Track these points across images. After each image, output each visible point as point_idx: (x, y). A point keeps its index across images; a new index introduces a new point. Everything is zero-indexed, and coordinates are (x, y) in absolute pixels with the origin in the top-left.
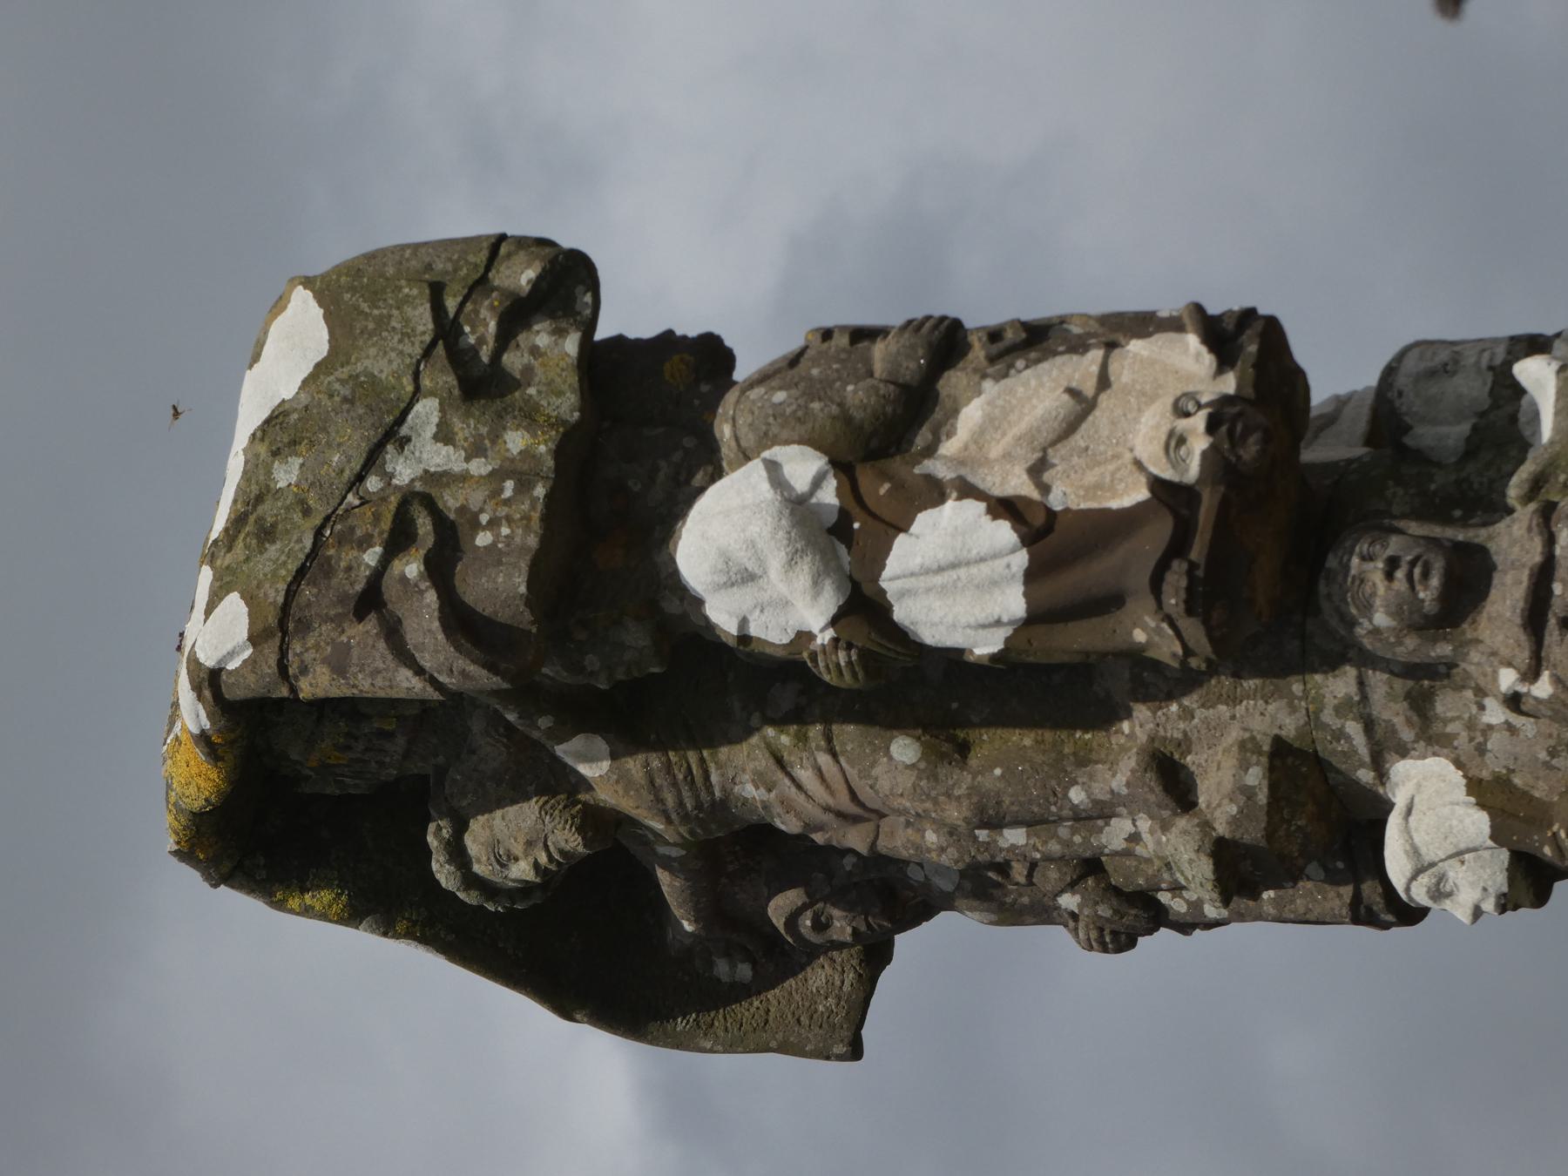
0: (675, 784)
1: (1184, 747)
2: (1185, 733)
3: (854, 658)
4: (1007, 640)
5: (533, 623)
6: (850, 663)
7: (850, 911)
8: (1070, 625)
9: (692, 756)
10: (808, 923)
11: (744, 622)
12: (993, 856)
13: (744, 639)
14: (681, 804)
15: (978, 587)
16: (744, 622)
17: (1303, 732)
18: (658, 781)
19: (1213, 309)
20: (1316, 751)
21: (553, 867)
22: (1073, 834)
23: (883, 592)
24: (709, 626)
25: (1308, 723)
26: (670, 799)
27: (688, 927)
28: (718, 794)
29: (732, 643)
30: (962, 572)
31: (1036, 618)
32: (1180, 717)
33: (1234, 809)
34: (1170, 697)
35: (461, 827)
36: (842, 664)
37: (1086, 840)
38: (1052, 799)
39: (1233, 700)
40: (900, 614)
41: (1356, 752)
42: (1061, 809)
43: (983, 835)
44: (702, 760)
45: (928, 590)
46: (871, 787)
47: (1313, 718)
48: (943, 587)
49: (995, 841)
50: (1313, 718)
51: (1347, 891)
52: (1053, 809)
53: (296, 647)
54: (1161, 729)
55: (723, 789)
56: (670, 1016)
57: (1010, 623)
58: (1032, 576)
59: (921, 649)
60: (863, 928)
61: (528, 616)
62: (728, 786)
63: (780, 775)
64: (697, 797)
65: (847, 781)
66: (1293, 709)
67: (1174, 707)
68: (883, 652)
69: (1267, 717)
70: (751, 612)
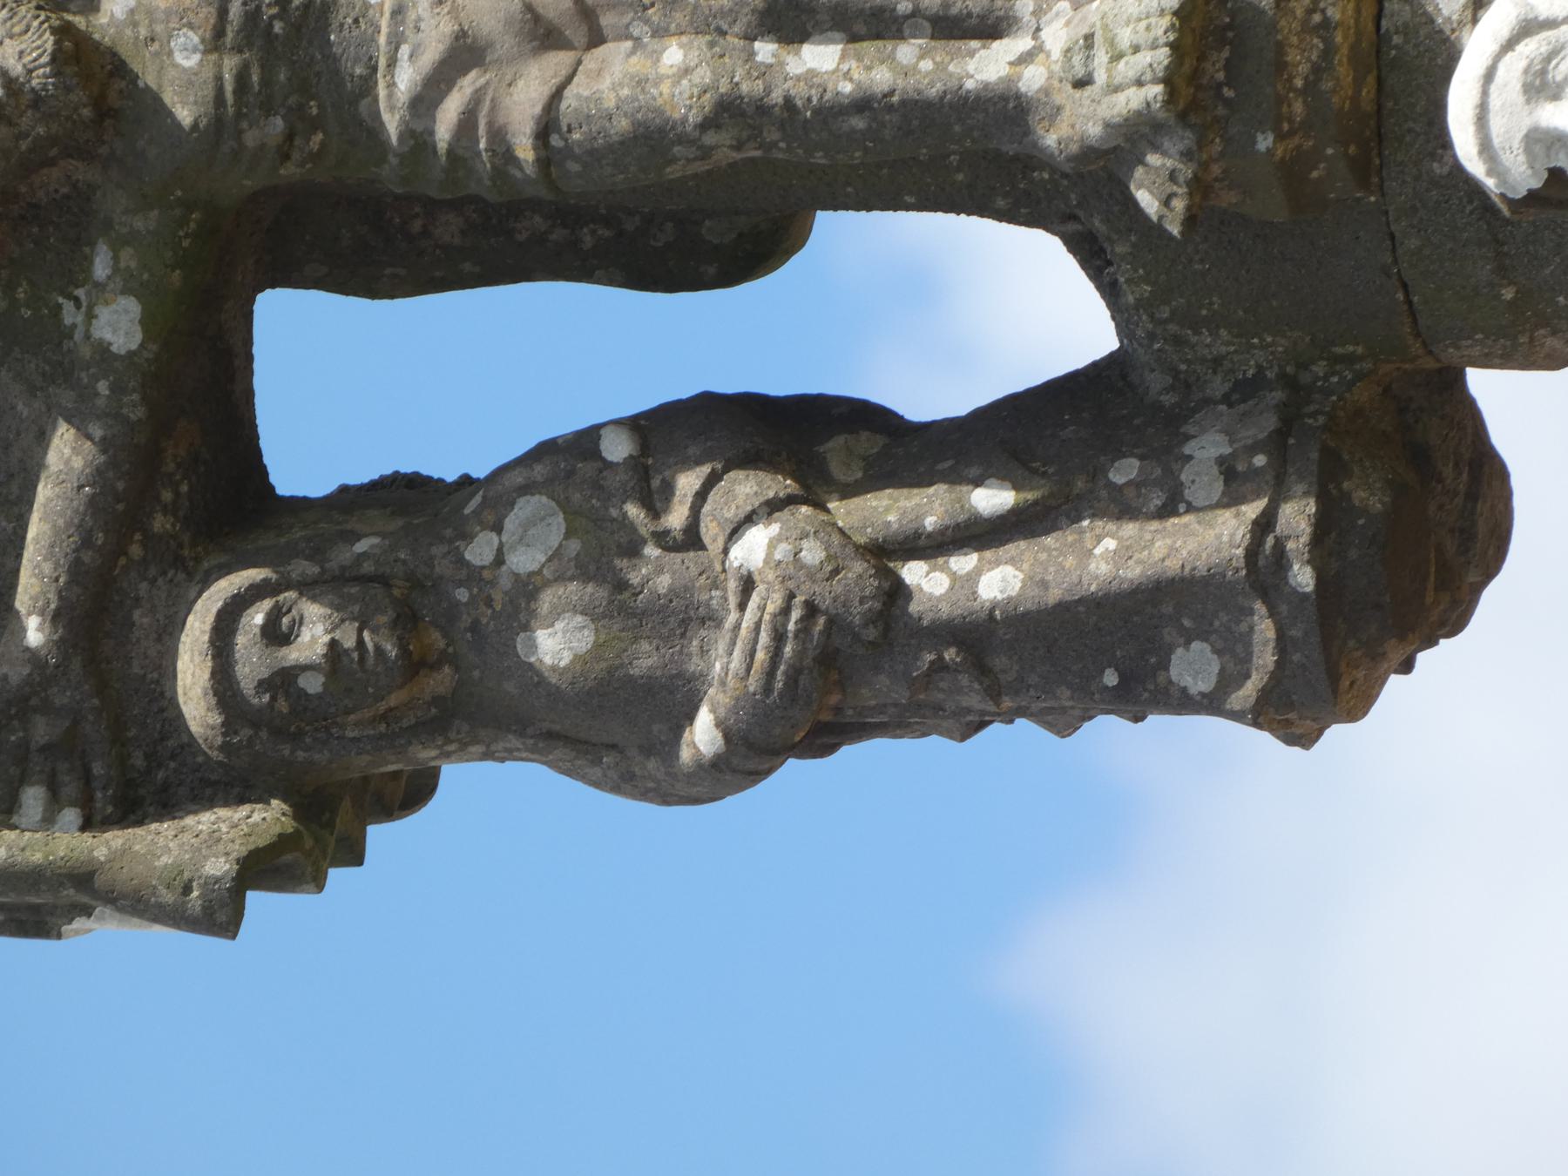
27: (35, 633)
43: (765, 50)
51: (1252, 510)
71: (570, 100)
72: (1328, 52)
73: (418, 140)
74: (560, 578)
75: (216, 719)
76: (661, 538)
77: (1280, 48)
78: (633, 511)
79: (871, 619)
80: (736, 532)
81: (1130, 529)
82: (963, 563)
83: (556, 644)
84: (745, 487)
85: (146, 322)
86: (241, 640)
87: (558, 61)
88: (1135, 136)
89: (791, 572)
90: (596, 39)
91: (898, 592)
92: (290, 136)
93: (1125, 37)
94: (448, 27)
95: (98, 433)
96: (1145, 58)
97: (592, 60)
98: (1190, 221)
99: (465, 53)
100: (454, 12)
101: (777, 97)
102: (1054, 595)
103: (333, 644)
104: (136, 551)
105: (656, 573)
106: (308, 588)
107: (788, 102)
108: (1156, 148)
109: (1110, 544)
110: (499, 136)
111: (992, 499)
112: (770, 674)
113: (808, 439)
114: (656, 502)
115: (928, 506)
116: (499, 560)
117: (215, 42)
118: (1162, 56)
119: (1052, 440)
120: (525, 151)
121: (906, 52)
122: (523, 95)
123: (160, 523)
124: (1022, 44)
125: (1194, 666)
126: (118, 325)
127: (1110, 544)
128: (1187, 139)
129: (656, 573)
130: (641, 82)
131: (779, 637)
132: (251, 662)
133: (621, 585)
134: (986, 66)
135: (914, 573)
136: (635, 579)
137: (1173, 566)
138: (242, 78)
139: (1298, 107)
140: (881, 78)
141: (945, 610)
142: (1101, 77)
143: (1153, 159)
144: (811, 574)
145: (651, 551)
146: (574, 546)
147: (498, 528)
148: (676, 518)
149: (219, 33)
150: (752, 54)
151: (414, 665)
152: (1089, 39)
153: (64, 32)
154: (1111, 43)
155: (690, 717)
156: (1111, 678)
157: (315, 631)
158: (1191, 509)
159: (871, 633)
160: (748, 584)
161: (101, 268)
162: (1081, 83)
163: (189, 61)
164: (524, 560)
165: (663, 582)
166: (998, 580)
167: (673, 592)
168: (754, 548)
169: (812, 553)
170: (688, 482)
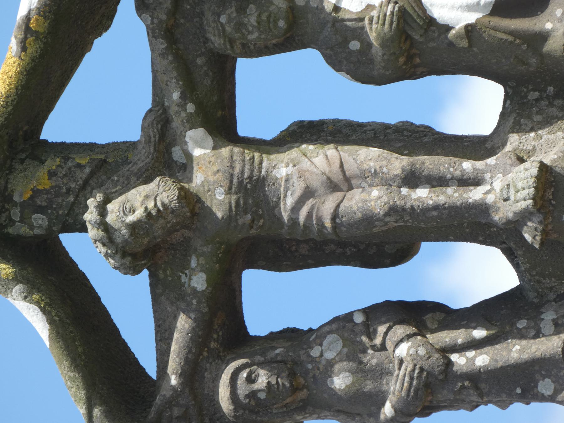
0: (243, 161)
2: (534, 147)
4: (478, 20)
6: (392, 13)
7: (270, 371)
8: (513, 20)
9: (257, 155)
10: (245, 375)
12: (405, 204)
14: (242, 172)
18: (235, 157)
21: (154, 213)
22: (455, 192)
26: (238, 167)
28: (263, 173)
34: (532, 130)
35: (108, 200)
36: (388, 13)
37: (461, 195)
38: (452, 164)
43: (404, 191)
44: (261, 156)
46: (354, 159)
49: (410, 195)
52: (452, 170)
54: (522, 145)
56: (237, 143)
57: (486, 5)
59: (431, 21)
60: (274, 382)
62: (270, 170)
63: (304, 158)
64: (252, 171)
65: (341, 158)
67: (532, 134)
68: (411, 12)
73: (294, 221)
74: (341, 360)
75: (232, 407)
76: (373, 347)
78: (364, 339)
79: (441, 372)
80: (397, 345)
81: (524, 342)
82: (471, 354)
83: (340, 382)
84: (400, 331)
85: (208, 281)
86: (239, 382)
87: (338, 196)
88: (524, 216)
89: (415, 357)
90: (350, 188)
91: (449, 364)
92: (253, 221)
93: (520, 185)
94: (303, 185)
95: (193, 316)
96: (526, 191)
97: (349, 195)
98: (542, 243)
99: (308, 193)
100: (305, 180)
101: (408, 205)
102: (500, 364)
103: (269, 383)
104: (205, 354)
105: (372, 358)
106: (261, 365)
108: (531, 220)
109: (518, 347)
110: (320, 220)
111: (479, 333)
112: (409, 390)
113: (420, 315)
114: (371, 335)
115: (459, 336)
116: (321, 355)
117: (229, 191)
118: (532, 191)
119: (499, 315)
120: (328, 224)
121: (450, 190)
122: (327, 206)
123: (213, 345)
125: (546, 386)
126: (199, 282)
127: (518, 347)
128: (541, 217)
129: (372, 358)
130: (365, 201)
131: (412, 379)
132: (243, 389)
133: (361, 363)
134: (475, 194)
135: (454, 357)
136: (365, 360)
137: (538, 354)
138: (237, 203)
140: (442, 199)
141: (465, 369)
142: (512, 198)
143: (530, 224)
144: (422, 358)
145: (370, 351)
146: (345, 350)
147: (321, 345)
148: (378, 341)
149: (230, 188)
151: (295, 389)
152: (508, 185)
153: (181, 189)
154: (515, 187)
155: (383, 404)
156: (519, 391)
157: (263, 379)
158: (544, 336)
159: (441, 377)
160: (401, 362)
161: (193, 264)
162: (506, 200)
163: (221, 197)
164: (330, 355)
165: (374, 361)
166: (482, 359)
167: (377, 365)
168: (403, 350)
169: (422, 351)
170: (382, 329)
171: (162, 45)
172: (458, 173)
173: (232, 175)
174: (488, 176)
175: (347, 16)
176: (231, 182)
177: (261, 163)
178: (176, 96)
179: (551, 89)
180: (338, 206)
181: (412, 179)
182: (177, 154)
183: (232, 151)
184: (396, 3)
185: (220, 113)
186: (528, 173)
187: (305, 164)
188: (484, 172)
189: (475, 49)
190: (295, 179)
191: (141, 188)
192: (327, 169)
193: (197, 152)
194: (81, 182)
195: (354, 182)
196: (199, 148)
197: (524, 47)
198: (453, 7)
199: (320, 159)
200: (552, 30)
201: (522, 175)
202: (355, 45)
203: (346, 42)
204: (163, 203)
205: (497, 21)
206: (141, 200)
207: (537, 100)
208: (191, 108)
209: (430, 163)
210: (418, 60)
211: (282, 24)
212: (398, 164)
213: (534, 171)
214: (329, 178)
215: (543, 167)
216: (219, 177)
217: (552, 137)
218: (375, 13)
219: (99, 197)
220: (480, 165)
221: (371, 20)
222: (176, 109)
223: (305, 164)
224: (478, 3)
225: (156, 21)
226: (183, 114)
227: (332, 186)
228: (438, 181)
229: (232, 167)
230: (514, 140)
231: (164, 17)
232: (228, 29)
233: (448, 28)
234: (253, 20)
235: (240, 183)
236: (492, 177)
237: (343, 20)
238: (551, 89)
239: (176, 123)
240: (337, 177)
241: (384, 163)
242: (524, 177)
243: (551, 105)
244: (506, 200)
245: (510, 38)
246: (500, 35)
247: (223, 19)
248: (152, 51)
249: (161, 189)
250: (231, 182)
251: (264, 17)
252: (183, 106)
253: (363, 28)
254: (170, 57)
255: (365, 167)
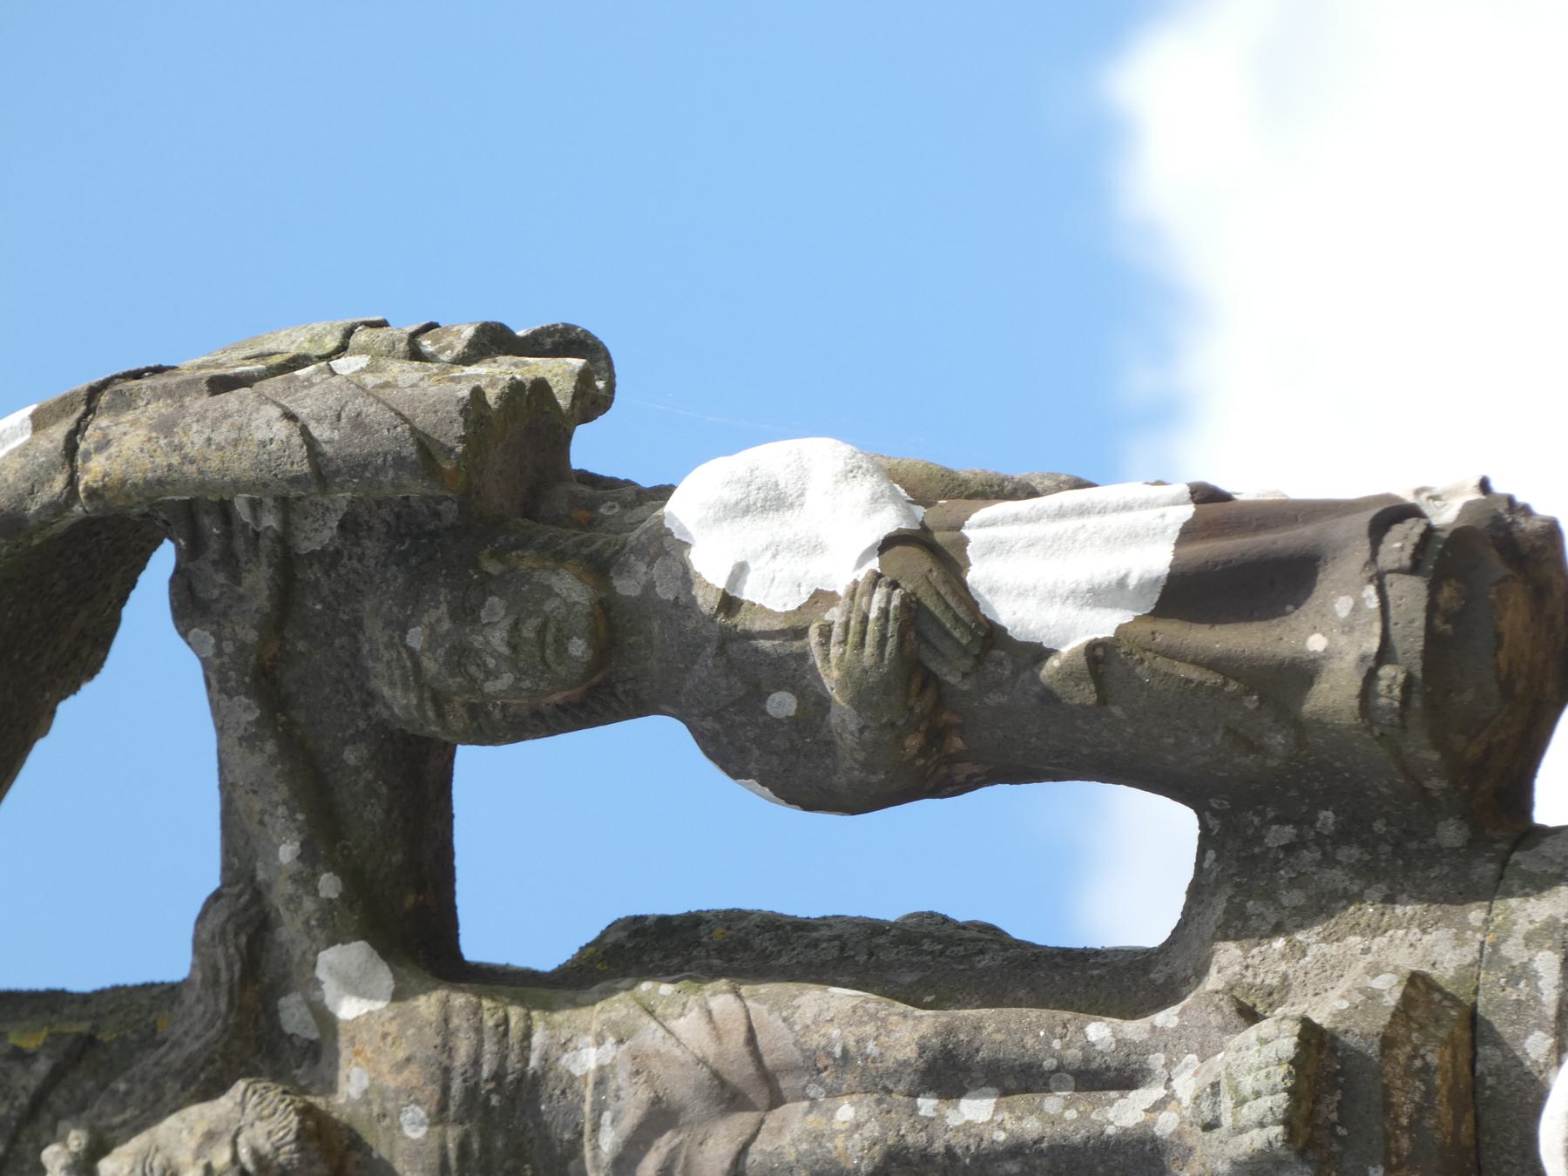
0: (479, 1030)
1: (1276, 996)
2: (1285, 977)
3: (896, 602)
5: (462, 439)
6: (885, 612)
9: (515, 1013)
11: (740, 571)
12: (931, 1141)
13: (729, 603)
14: (476, 1062)
15: (1107, 540)
16: (740, 571)
17: (1469, 974)
18: (455, 1022)
19: (1498, 487)
20: (1475, 1005)
22: (1067, 1108)
23: (964, 542)
24: (686, 577)
25: (1477, 963)
28: (534, 1062)
29: (707, 602)
30: (1092, 522)
31: (1186, 593)
32: (1283, 956)
33: (1345, 1004)
34: (1278, 930)
36: (873, 614)
38: (1059, 1030)
39: (1376, 930)
40: (977, 576)
41: (1538, 1001)
42: (1067, 1046)
43: (927, 1105)
44: (528, 1017)
45: (1031, 545)
47: (1489, 957)
48: (1057, 538)
49: (943, 1117)
50: (1489, 957)
52: (1057, 1044)
53: (103, 421)
55: (545, 1058)
57: (1143, 587)
58: (1188, 533)
59: (992, 635)
61: (458, 429)
62: (554, 1053)
63: (646, 1019)
64: (503, 1058)
66: (1459, 940)
67: (1279, 943)
69: (1419, 952)
70: (757, 557)
71: (754, 1156)
72: (1429, 1094)
77: (1386, 1090)
87: (742, 1122)
90: (777, 1100)
93: (1248, 1084)
94: (644, 1095)
96: (1266, 1102)
97: (773, 1119)
99: (660, 1117)
100: (650, 1081)
101: (939, 1146)
107: (949, 1151)
117: (439, 1115)
118: (1282, 1099)
121: (1053, 1103)
124: (1155, 1093)
130: (817, 1137)
134: (1125, 1113)
138: (463, 1147)
139: (1405, 1143)
140: (1031, 1127)
142: (1227, 1121)
149: (443, 1107)
150: (916, 1109)
152: (1215, 1086)
153: (307, 1112)
154: (1235, 1090)
162: (1209, 1127)
171: (247, 712)
172: (1074, 1055)
173: (447, 1071)
174: (1157, 1060)
175: (758, 626)
176: (445, 1090)
177: (527, 1035)
178: (287, 853)
179: (1327, 817)
180: (743, 1151)
181: (947, 1073)
182: (293, 1015)
183: (445, 1004)
184: (894, 585)
185: (410, 900)
186: (1269, 1052)
187: (650, 1035)
188: (1145, 1049)
189: (1116, 710)
190: (621, 1078)
191: (194, 1111)
192: (710, 1049)
193: (349, 1009)
194: (24, 1100)
195: (785, 1083)
196: (353, 994)
197: (1251, 702)
198: (1051, 596)
199: (690, 1022)
200: (1328, 655)
201: (1252, 1057)
202: (782, 704)
203: (758, 694)
204: (255, 1153)
205: (1173, 632)
206: (193, 1143)
207: (1289, 849)
208: (329, 885)
209: (996, 1027)
210: (957, 743)
211: (578, 648)
212: (907, 1031)
213: (1287, 1045)
214: (716, 1074)
215: (1311, 1035)
216: (412, 1075)
217: (1332, 949)
218: (835, 615)
219: (76, 1140)
220: (1135, 1029)
221: (826, 632)
222: (289, 888)
223: (650, 1035)
224: (1122, 583)
225: (229, 647)
226: (309, 904)
227: (727, 1096)
228: (1018, 1078)
229: (447, 1048)
230: (1228, 959)
231: (251, 636)
232: (430, 666)
233: (1038, 653)
234: (497, 639)
235: (471, 1092)
236: (1168, 1065)
237: (749, 635)
238: (1327, 817)
239: (290, 929)
240: (740, 1071)
241: (869, 1029)
242: (1259, 1060)
243: (1328, 861)
244: (1209, 1127)
245: (1213, 679)
246: (1183, 670)
247: (416, 638)
248: (220, 730)
249: (250, 1113)
250: (445, 1090)
251: (528, 631)
252: (306, 882)
253: (803, 656)
254: (270, 747)
255: (815, 1040)
